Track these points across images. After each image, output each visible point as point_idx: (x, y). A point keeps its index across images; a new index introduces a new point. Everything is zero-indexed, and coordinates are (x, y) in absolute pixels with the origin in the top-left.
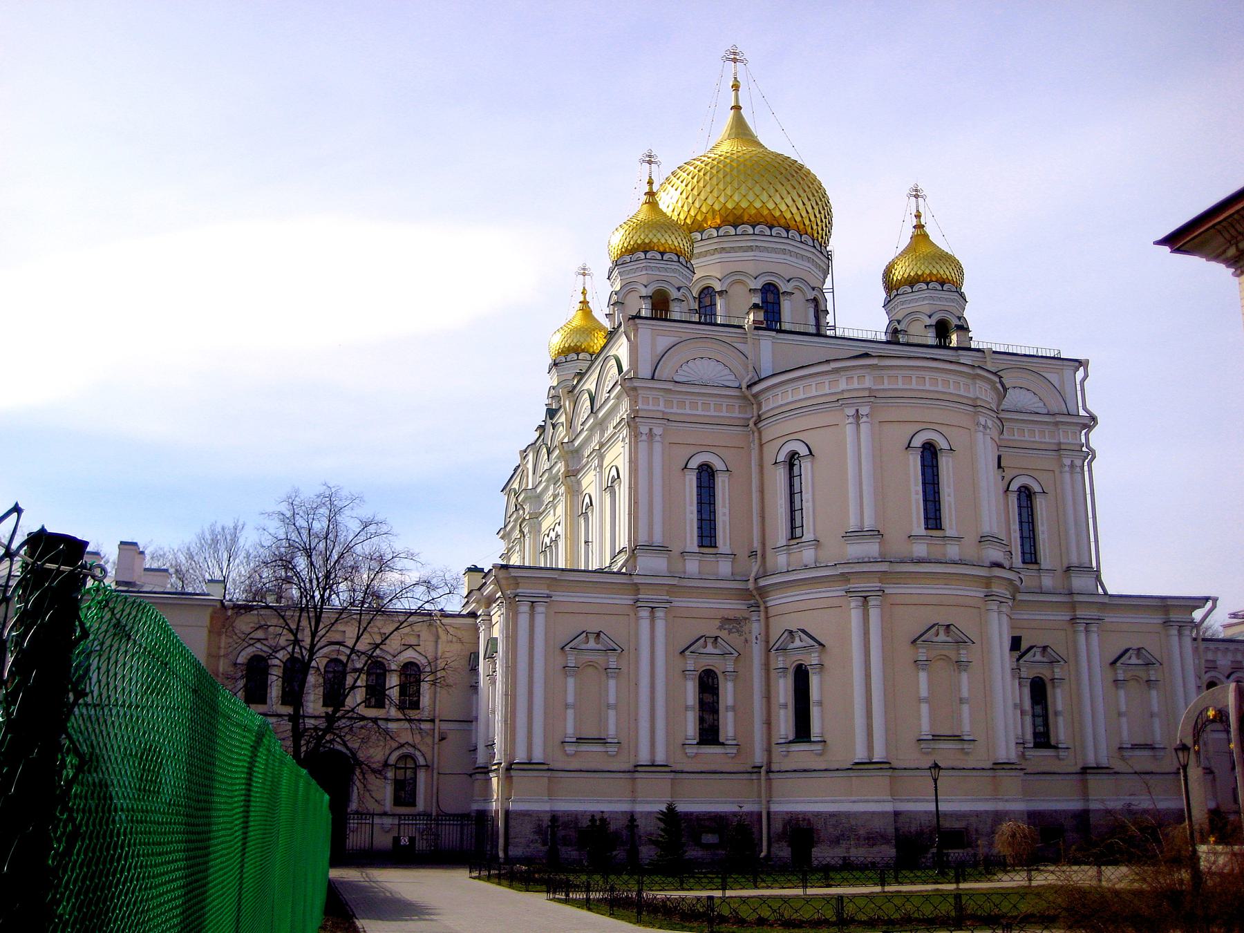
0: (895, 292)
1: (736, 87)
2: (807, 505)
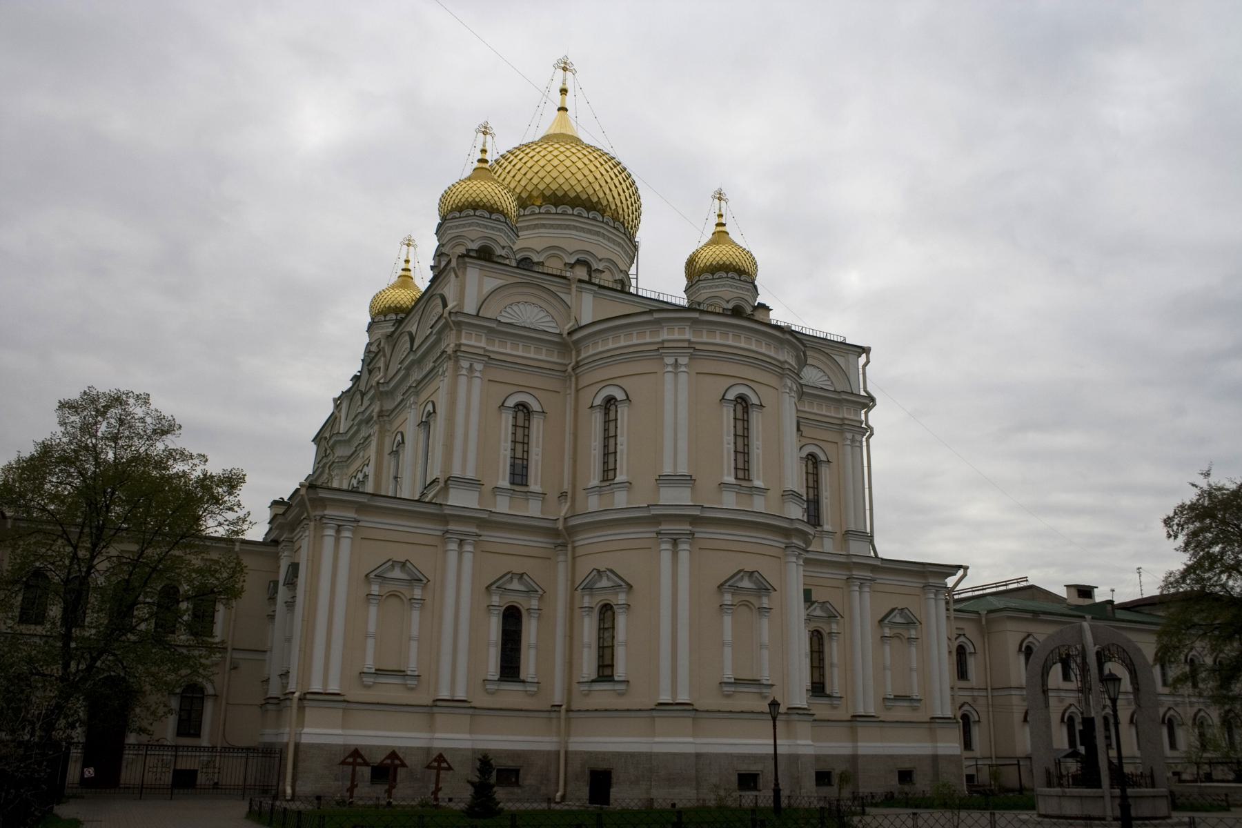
1: (564, 91)
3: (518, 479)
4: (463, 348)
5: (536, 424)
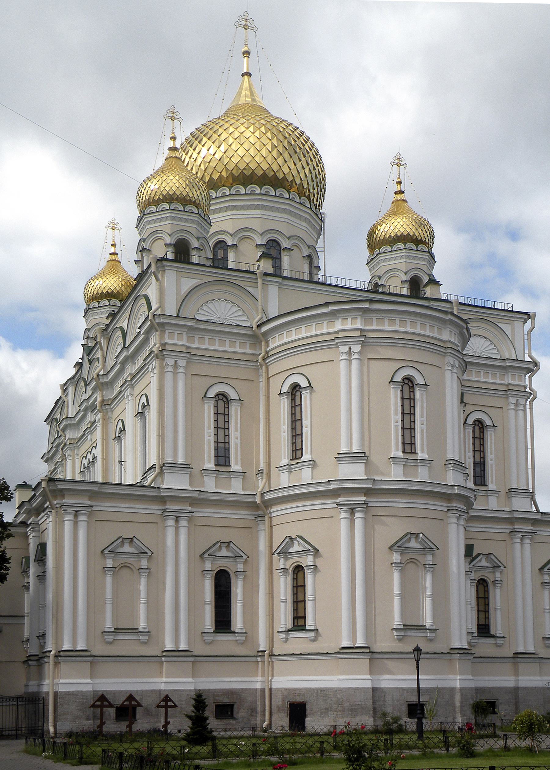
0: (377, 251)
2: (306, 430)
3: (222, 460)
4: (168, 348)
5: (235, 411)
